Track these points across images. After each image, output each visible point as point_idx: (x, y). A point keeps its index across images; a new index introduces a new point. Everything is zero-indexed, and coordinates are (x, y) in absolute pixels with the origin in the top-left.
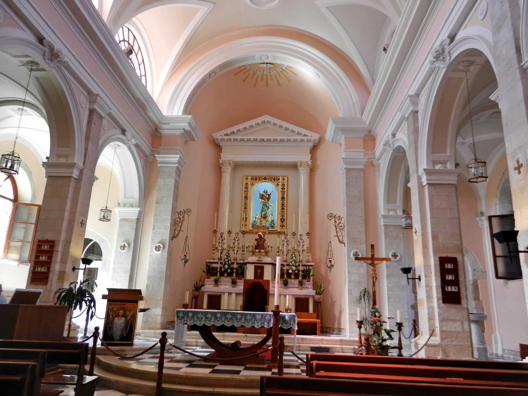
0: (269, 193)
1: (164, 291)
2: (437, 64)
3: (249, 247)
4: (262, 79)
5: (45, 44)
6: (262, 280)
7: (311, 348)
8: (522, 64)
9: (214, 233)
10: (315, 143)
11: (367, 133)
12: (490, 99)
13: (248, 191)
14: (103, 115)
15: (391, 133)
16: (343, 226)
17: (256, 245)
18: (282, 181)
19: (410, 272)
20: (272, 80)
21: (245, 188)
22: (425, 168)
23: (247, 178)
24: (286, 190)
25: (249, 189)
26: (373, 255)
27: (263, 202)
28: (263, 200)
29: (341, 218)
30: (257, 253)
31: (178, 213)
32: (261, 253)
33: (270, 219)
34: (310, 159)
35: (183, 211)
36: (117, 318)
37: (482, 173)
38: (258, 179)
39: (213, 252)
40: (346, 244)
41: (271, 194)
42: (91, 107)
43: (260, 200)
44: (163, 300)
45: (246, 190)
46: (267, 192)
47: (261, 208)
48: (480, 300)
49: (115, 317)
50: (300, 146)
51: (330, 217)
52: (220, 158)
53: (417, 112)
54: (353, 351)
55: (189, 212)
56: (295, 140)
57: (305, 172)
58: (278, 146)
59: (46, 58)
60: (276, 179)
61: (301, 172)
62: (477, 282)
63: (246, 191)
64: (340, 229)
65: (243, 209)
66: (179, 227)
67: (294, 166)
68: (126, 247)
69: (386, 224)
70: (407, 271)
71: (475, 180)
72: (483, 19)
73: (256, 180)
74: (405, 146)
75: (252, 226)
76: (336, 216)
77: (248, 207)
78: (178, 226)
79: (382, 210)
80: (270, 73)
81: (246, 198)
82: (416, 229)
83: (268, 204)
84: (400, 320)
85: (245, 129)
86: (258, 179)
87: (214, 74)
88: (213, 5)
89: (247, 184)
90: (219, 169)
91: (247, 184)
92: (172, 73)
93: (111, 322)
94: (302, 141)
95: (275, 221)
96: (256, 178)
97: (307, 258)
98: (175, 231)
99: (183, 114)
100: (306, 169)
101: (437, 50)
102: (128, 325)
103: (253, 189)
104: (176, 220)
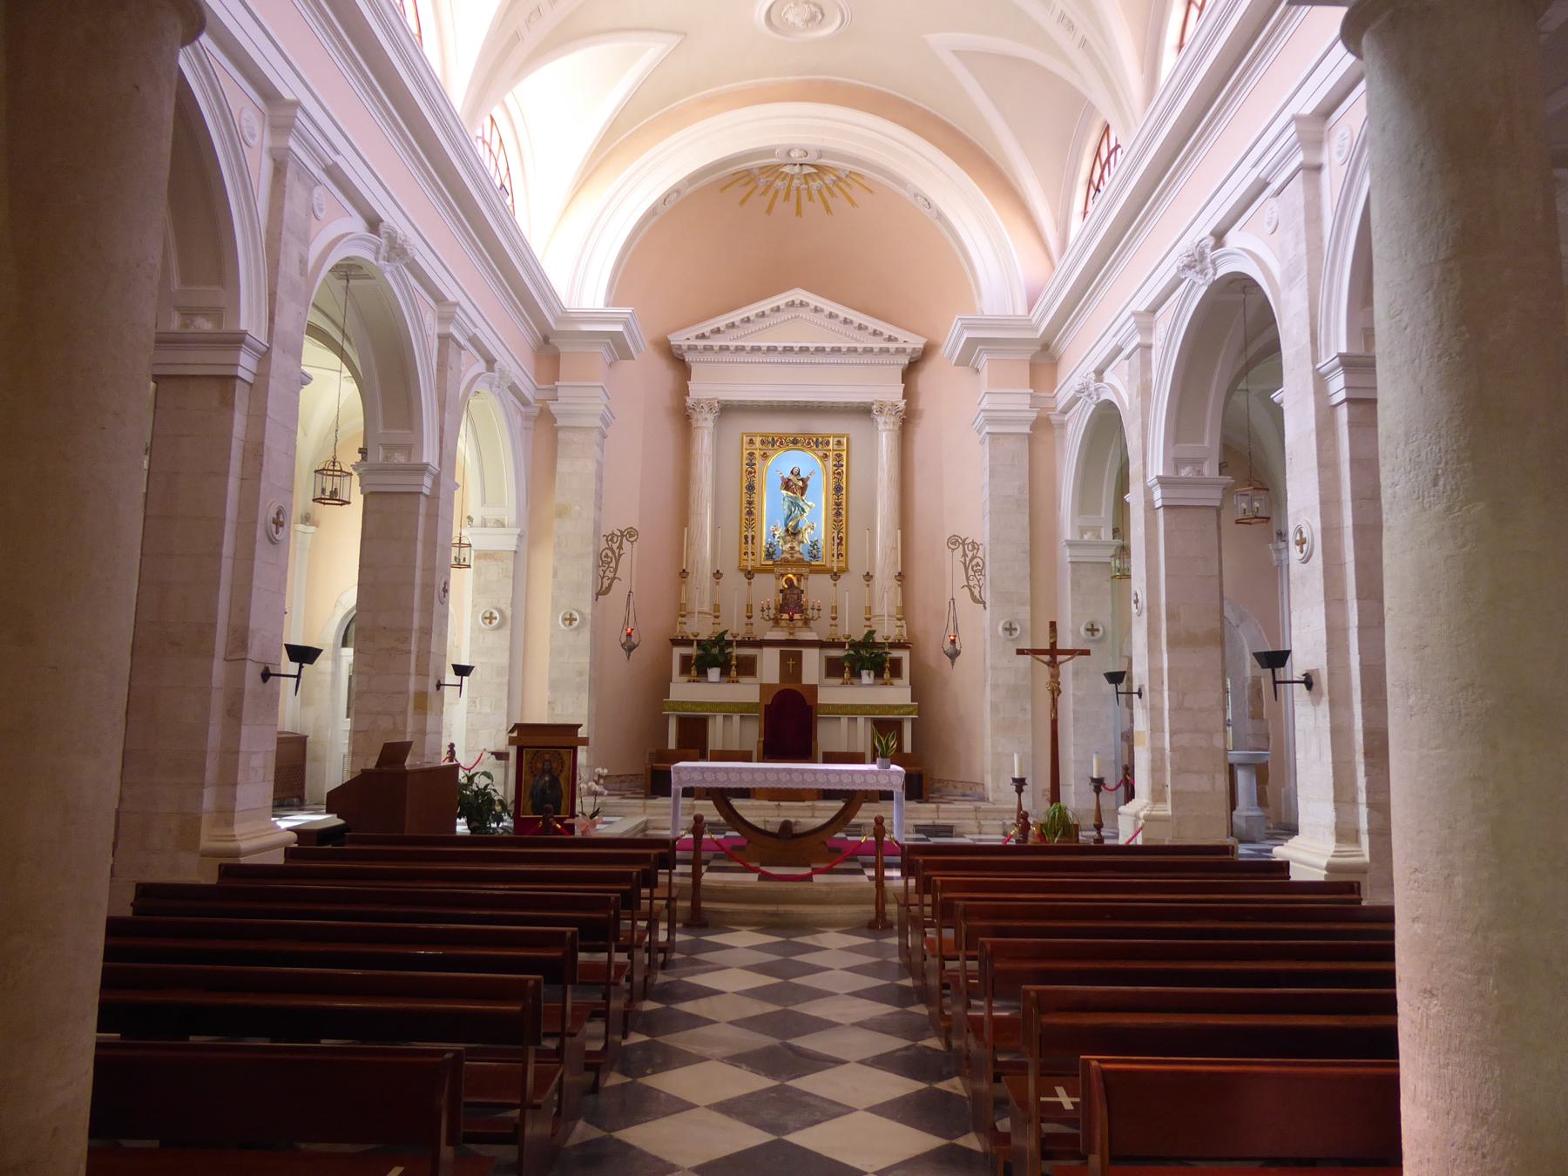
0: (803, 475)
1: (589, 715)
2: (1190, 275)
3: (769, 609)
6: (799, 684)
7: (915, 826)
8: (1318, 366)
10: (914, 356)
11: (1039, 348)
13: (755, 472)
14: (462, 341)
16: (981, 563)
18: (836, 447)
19: (1121, 681)
20: (810, 199)
22: (1161, 474)
23: (751, 440)
24: (844, 468)
25: (756, 467)
26: (1053, 644)
28: (790, 494)
29: (978, 546)
30: (783, 622)
31: (607, 537)
33: (807, 537)
34: (901, 397)
38: (778, 444)
40: (988, 605)
41: (808, 478)
42: (444, 331)
43: (784, 492)
45: (750, 469)
46: (799, 474)
47: (786, 512)
53: (1150, 347)
54: (1001, 830)
59: (381, 256)
60: (821, 443)
61: (881, 427)
62: (1260, 681)
63: (750, 473)
64: (975, 572)
66: (612, 570)
67: (864, 411)
70: (1115, 678)
73: (773, 446)
76: (967, 542)
77: (754, 511)
79: (1067, 531)
81: (751, 488)
82: (1136, 595)
83: (803, 501)
84: (1099, 772)
86: (778, 444)
87: (675, 194)
88: (676, 39)
89: (751, 454)
90: (684, 417)
91: (751, 454)
92: (574, 192)
95: (821, 544)
96: (773, 439)
98: (602, 579)
99: (607, 305)
100: (892, 419)
101: (1190, 253)
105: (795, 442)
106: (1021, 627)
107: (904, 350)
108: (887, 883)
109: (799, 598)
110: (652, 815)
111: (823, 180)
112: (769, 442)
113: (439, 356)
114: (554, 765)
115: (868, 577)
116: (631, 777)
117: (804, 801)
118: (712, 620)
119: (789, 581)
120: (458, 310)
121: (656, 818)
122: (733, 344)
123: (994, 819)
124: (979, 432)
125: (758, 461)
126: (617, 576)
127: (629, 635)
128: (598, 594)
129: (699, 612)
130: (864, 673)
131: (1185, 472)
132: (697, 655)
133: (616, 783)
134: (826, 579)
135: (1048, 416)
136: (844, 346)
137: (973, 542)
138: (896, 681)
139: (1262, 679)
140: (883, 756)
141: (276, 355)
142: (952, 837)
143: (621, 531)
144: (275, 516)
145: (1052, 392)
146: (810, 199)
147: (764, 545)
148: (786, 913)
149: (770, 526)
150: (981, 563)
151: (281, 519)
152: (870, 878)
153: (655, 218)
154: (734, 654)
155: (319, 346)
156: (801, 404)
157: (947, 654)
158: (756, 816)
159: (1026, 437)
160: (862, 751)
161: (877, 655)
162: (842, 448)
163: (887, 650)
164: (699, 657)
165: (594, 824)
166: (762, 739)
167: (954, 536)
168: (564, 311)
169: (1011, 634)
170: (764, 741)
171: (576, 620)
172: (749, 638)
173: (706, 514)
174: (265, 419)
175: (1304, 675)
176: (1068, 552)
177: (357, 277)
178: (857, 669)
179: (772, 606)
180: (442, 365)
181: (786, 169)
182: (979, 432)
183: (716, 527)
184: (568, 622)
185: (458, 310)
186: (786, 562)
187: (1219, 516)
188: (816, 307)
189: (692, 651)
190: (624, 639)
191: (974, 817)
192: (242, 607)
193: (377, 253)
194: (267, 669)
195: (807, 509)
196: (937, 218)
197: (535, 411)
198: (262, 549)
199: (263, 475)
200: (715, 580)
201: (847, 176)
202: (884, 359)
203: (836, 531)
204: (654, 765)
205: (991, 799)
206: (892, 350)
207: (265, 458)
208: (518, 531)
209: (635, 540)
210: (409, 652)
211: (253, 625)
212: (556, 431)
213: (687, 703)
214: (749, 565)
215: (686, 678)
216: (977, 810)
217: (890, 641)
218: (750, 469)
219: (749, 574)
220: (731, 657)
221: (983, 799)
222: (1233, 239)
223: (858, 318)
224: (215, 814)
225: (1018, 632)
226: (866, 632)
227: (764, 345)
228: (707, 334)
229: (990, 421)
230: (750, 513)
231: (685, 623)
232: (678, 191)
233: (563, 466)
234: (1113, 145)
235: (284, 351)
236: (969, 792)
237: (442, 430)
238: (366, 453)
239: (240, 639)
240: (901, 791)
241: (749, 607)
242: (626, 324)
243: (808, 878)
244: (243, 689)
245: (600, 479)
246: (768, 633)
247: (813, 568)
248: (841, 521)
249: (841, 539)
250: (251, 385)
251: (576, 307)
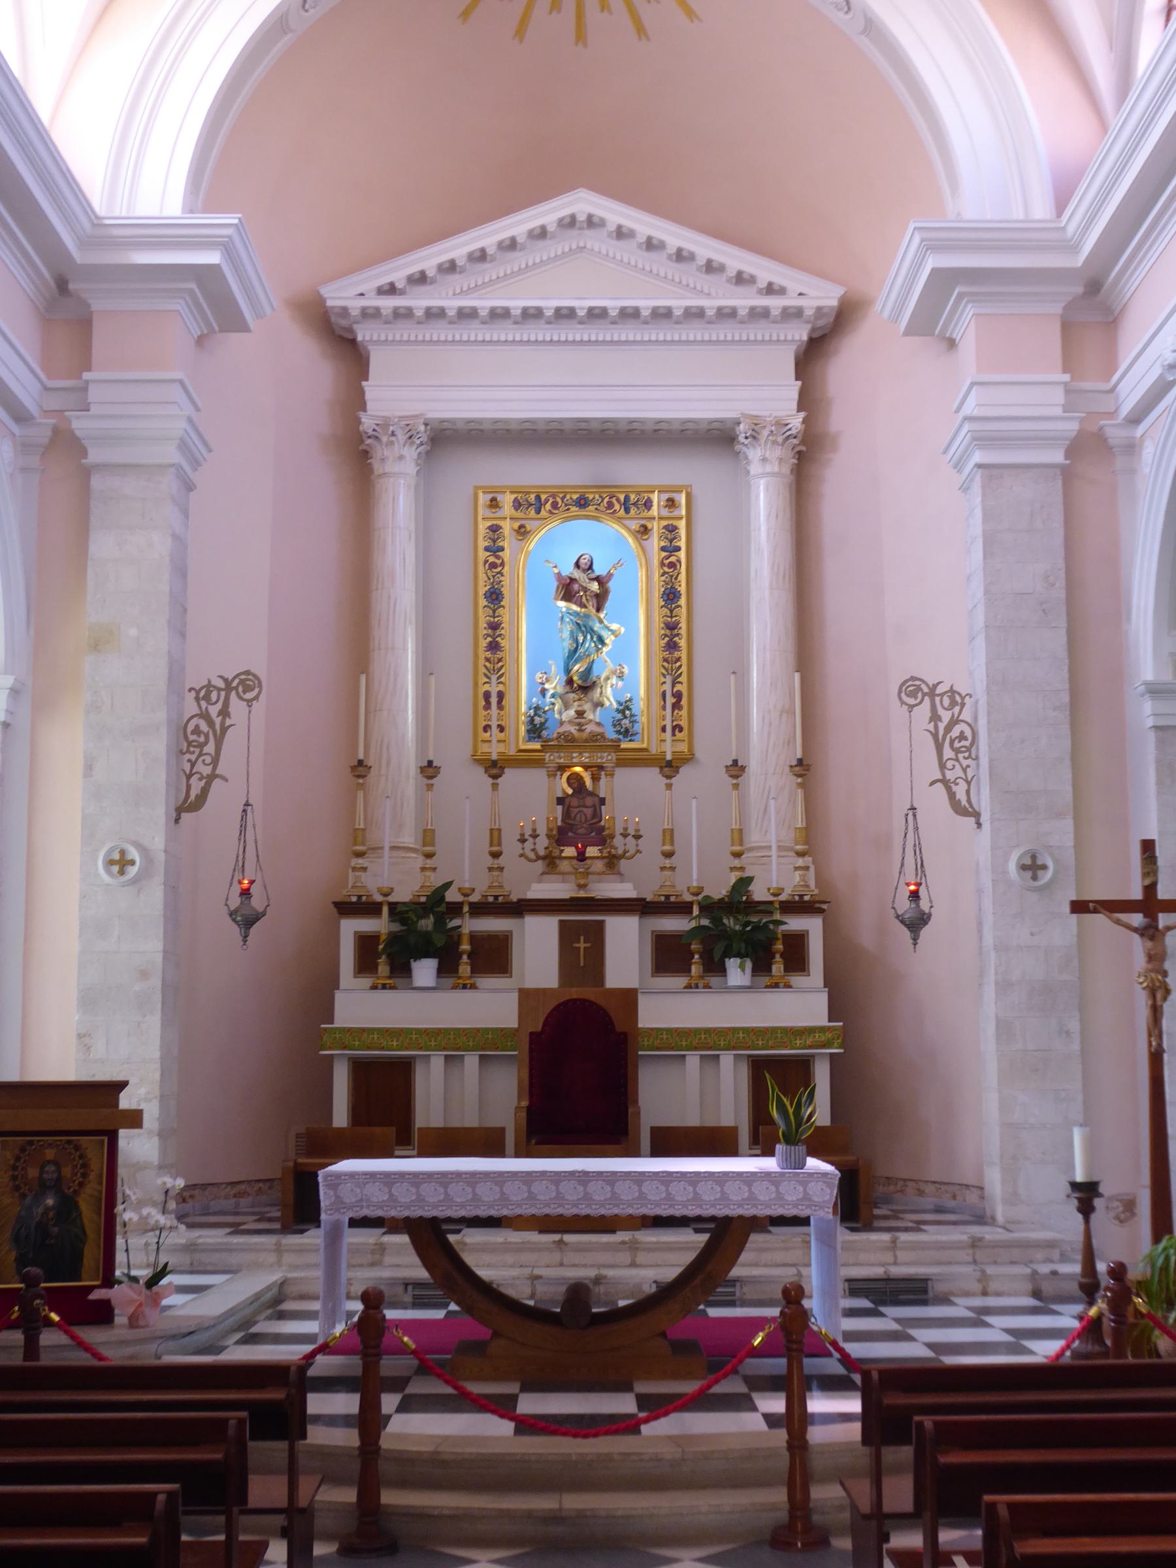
0: (599, 570)
1: (162, 1058)
9: (359, 777)
10: (821, 323)
11: (1079, 290)
13: (502, 564)
16: (968, 733)
18: (665, 512)
21: (487, 549)
23: (493, 500)
24: (682, 555)
25: (506, 555)
26: (1150, 889)
27: (577, 614)
28: (575, 608)
29: (963, 698)
31: (198, 692)
32: (588, 862)
33: (609, 694)
34: (794, 405)
35: (221, 684)
38: (548, 506)
40: (985, 818)
41: (610, 576)
43: (562, 604)
44: (162, 1096)
45: (492, 559)
46: (591, 567)
47: (567, 644)
50: (748, 340)
51: (913, 694)
52: (363, 407)
54: (1029, 1287)
55: (248, 689)
56: (727, 315)
57: (776, 469)
58: (642, 342)
61: (755, 468)
63: (493, 566)
64: (957, 751)
65: (483, 654)
66: (208, 759)
69: (1162, 722)
73: (538, 511)
75: (528, 731)
76: (939, 690)
77: (503, 643)
78: (201, 754)
81: (495, 596)
83: (601, 622)
85: (481, 256)
86: (548, 506)
89: (495, 529)
91: (495, 529)
94: (761, 314)
95: (639, 706)
96: (538, 498)
97: (797, 879)
98: (189, 777)
99: (189, 209)
100: (778, 452)
103: (528, 553)
105: (582, 503)
106: (1056, 861)
107: (798, 313)
108: (816, 1435)
109: (597, 815)
110: (297, 1267)
114: (67, 1171)
115: (736, 769)
117: (613, 1232)
118: (420, 861)
119: (575, 780)
121: (302, 1274)
122: (452, 304)
123: (1013, 1263)
124: (958, 466)
125: (508, 542)
126: (217, 772)
127: (246, 893)
128: (180, 810)
129: (393, 848)
130: (732, 964)
132: (390, 933)
133: (227, 1197)
134: (651, 777)
135: (1101, 428)
136: (678, 304)
138: (797, 980)
140: (790, 1140)
142: (924, 1303)
145: (1108, 380)
147: (523, 708)
148: (581, 1515)
150: (968, 733)
152: (771, 1420)
153: (288, 39)
154: (466, 930)
156: (594, 426)
157: (902, 922)
158: (512, 1266)
159: (1059, 473)
160: (732, 1124)
161: (757, 928)
162: (676, 513)
163: (777, 916)
164: (393, 938)
165: (156, 1301)
166: (525, 1103)
167: (913, 678)
168: (97, 222)
169: (1035, 878)
170: (529, 1108)
171: (132, 863)
172: (496, 897)
173: (405, 649)
176: (1148, 706)
178: (717, 957)
179: (542, 830)
182: (958, 466)
183: (426, 671)
184: (116, 868)
186: (568, 742)
188: (619, 227)
189: (379, 925)
190: (235, 902)
191: (970, 1259)
195: (609, 639)
196: (863, 32)
197: (41, 434)
202: (757, 331)
203: (669, 679)
204: (300, 1160)
205: (1000, 1218)
206: (775, 312)
208: (9, 681)
212: (86, 473)
213: (409, 1031)
214: (494, 751)
215: (366, 982)
216: (975, 1243)
217: (783, 897)
218: (492, 559)
219: (495, 768)
220: (460, 936)
221: (982, 1218)
223: (705, 248)
225: (1049, 874)
226: (733, 881)
227: (517, 305)
229: (982, 440)
231: (364, 869)
233: (102, 546)
236: (951, 1204)
240: (831, 1216)
241: (495, 835)
242: (227, 248)
243: (627, 1425)
245: (180, 570)
246: (535, 886)
247: (622, 755)
248: (678, 659)
249: (678, 696)
251: (124, 214)
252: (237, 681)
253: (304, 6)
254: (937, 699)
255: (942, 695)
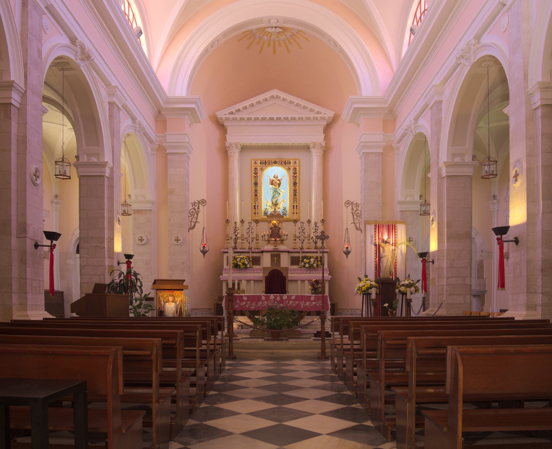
2: (463, 61)
3: (265, 236)
4: (269, 45)
5: (78, 44)
10: (329, 120)
12: (503, 112)
13: (258, 177)
15: (412, 118)
16: (360, 212)
17: (271, 233)
18: (294, 165)
20: (280, 45)
22: (446, 161)
23: (255, 162)
24: (297, 174)
25: (258, 175)
29: (359, 205)
30: (272, 242)
31: (192, 204)
34: (323, 140)
35: (197, 202)
36: (167, 303)
37: (493, 171)
38: (268, 163)
39: (228, 242)
41: (281, 179)
45: (255, 175)
46: (277, 177)
47: (272, 195)
48: (484, 278)
49: (166, 303)
51: (348, 204)
52: (226, 140)
55: (203, 203)
56: (308, 119)
57: (319, 155)
61: (314, 154)
62: (483, 262)
63: (255, 177)
64: (357, 216)
65: (253, 197)
67: (307, 148)
68: (177, 242)
71: (487, 177)
72: (504, 32)
73: (265, 165)
74: (428, 132)
76: (354, 203)
78: (193, 217)
80: (278, 37)
81: (256, 184)
83: (279, 190)
86: (268, 163)
87: (217, 42)
89: (256, 169)
90: (225, 152)
91: (256, 169)
93: (163, 307)
95: (288, 209)
96: (265, 161)
98: (191, 222)
101: (463, 49)
102: (178, 309)
104: (191, 212)
107: (324, 118)
109: (279, 231)
111: (286, 36)
112: (264, 163)
113: (109, 112)
116: (207, 310)
120: (117, 90)
122: (246, 117)
125: (259, 172)
126: (197, 221)
127: (204, 247)
128: (189, 229)
131: (457, 160)
135: (391, 144)
137: (356, 203)
139: (484, 261)
141: (29, 93)
143: (198, 201)
144: (35, 172)
146: (280, 45)
149: (266, 204)
150: (360, 212)
151: (38, 174)
155: (54, 110)
162: (296, 165)
167: (348, 201)
174: (26, 126)
175: (514, 238)
177: (67, 69)
180: (111, 117)
181: (268, 30)
183: (241, 200)
185: (117, 90)
187: (471, 180)
190: (202, 249)
192: (23, 213)
193: (76, 56)
194: (37, 243)
195: (281, 194)
198: (29, 186)
199: (27, 152)
200: (241, 224)
201: (297, 33)
207: (28, 144)
209: (205, 205)
210: (104, 248)
211: (28, 222)
218: (255, 175)
222: (486, 39)
223: (303, 103)
224: (18, 306)
227: (260, 117)
228: (234, 112)
230: (256, 195)
232: (218, 41)
234: (423, 10)
235: (33, 94)
237: (113, 147)
238: (79, 158)
239: (23, 228)
244: (26, 251)
250: (19, 109)
251: (173, 96)
252: (201, 201)
253: (212, 47)
254: (353, 205)
255: (354, 204)
